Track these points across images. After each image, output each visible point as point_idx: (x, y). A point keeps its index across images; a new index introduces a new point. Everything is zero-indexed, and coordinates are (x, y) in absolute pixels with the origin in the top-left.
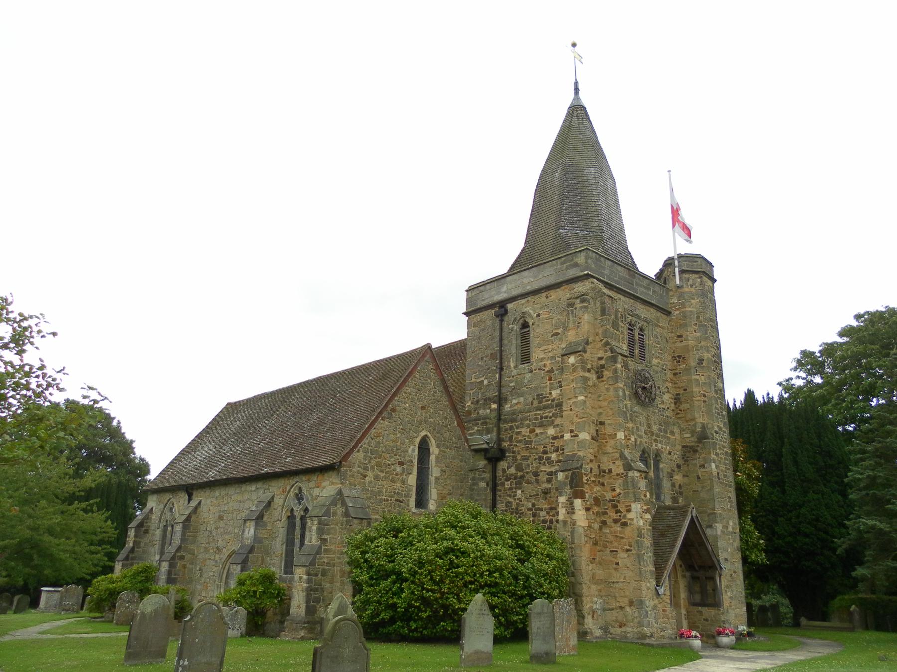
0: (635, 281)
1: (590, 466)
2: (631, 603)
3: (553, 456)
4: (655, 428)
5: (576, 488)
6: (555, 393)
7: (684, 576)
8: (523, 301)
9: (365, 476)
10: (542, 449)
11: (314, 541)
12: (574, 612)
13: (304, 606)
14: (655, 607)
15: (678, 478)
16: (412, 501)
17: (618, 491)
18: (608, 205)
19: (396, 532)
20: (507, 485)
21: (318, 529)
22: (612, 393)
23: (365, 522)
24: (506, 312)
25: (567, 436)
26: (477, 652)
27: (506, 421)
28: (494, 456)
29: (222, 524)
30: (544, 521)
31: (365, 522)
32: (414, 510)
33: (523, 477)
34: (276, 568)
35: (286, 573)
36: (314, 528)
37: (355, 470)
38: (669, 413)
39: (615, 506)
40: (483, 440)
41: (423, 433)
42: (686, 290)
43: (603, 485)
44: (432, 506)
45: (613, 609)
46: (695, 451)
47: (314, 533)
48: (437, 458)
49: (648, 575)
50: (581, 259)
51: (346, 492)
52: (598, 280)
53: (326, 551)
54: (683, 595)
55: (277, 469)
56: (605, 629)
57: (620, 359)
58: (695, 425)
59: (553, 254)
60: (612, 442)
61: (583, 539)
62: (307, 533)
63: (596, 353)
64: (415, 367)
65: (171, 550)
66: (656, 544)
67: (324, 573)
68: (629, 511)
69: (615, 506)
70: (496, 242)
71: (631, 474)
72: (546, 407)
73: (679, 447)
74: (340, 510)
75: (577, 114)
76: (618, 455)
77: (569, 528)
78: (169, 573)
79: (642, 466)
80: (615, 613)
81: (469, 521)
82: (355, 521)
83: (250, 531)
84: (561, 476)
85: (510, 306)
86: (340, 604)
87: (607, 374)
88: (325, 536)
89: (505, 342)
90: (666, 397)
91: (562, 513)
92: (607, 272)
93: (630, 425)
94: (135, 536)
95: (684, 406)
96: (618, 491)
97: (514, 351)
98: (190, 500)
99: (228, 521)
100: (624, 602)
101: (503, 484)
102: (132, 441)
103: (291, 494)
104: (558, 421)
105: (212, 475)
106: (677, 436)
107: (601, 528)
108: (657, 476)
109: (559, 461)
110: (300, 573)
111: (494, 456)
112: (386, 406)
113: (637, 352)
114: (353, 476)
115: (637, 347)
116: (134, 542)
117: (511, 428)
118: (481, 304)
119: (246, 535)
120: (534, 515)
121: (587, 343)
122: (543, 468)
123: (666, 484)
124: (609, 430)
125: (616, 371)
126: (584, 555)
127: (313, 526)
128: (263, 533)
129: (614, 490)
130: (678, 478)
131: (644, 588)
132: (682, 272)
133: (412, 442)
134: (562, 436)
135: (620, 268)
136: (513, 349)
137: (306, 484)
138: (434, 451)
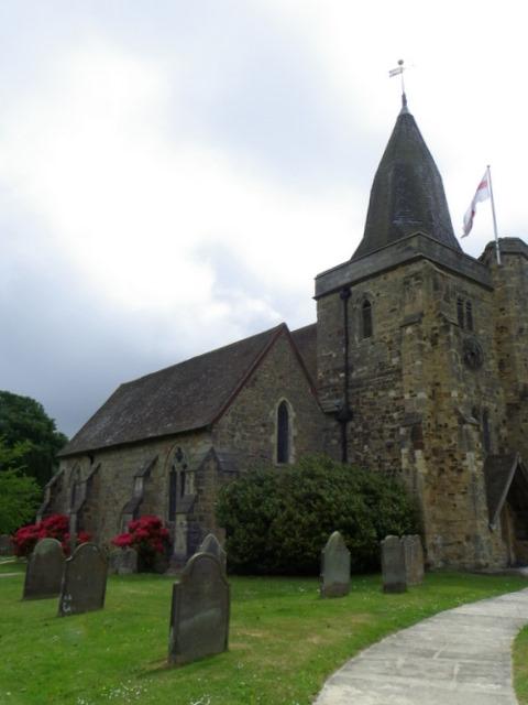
0: (463, 261)
1: (429, 421)
2: (468, 538)
3: (395, 415)
4: (483, 388)
5: (416, 439)
6: (395, 361)
7: (511, 515)
8: (365, 283)
9: (233, 436)
10: (384, 409)
11: (192, 493)
12: (420, 547)
13: (185, 547)
14: (489, 541)
15: (504, 431)
16: (275, 457)
17: (454, 442)
18: (436, 199)
19: (260, 483)
20: (356, 441)
21: (195, 481)
22: (445, 357)
23: (234, 475)
24: (350, 294)
25: (407, 396)
26: (335, 584)
27: (353, 387)
28: (343, 417)
29: (117, 481)
30: (389, 471)
31: (234, 475)
32: (277, 465)
33: (369, 434)
34: (162, 516)
35: (171, 519)
36: (192, 481)
37: (225, 430)
38: (495, 376)
39: (451, 456)
40: (333, 404)
41: (281, 399)
42: (507, 268)
43: (440, 438)
44: (292, 460)
45: (451, 544)
46: (518, 408)
47: (191, 484)
48: (295, 420)
49: (482, 514)
50: (414, 243)
51: (217, 449)
52: (430, 260)
53: (204, 499)
54: (511, 531)
55: (160, 433)
56: (446, 561)
57: (452, 328)
58: (517, 386)
59: (389, 242)
60: (446, 401)
61: (424, 484)
62: (186, 485)
63: (428, 324)
64: (273, 343)
65: (78, 503)
66: (488, 488)
67: (201, 518)
68: (464, 459)
69: (451, 456)
70: (336, 230)
71: (465, 427)
72: (387, 373)
73: (503, 405)
74: (213, 465)
75: (406, 123)
76: (452, 411)
77: (411, 475)
78: (78, 523)
79: (474, 420)
80: (454, 547)
81: (320, 470)
82: (226, 474)
83: (139, 486)
84: (402, 431)
85: (353, 289)
86: (214, 541)
87: (441, 341)
88: (201, 488)
89: (350, 320)
90: (492, 362)
91: (405, 462)
92: (437, 254)
93: (463, 385)
94: (52, 494)
95: (507, 370)
96: (454, 442)
97: (357, 327)
98: (92, 462)
99: (121, 479)
100: (461, 538)
101: (352, 441)
102: (53, 420)
103: (172, 455)
104: (398, 384)
105: (108, 441)
106: (502, 396)
107: (439, 475)
108: (486, 430)
109: (400, 419)
110: (181, 519)
111: (343, 417)
112: (250, 376)
113: (465, 324)
114: (222, 436)
115: (465, 319)
116: (51, 499)
117: (358, 393)
118: (327, 289)
119: (137, 489)
120: (380, 466)
121: (422, 315)
122: (386, 426)
123: (493, 436)
124: (444, 390)
125: (448, 339)
126: (425, 496)
127: (190, 479)
128: (150, 487)
129: (450, 441)
130: (504, 431)
131: (479, 525)
132: (502, 253)
133: (272, 407)
134: (403, 397)
135: (448, 251)
136: (356, 324)
137: (183, 445)
138: (292, 414)
